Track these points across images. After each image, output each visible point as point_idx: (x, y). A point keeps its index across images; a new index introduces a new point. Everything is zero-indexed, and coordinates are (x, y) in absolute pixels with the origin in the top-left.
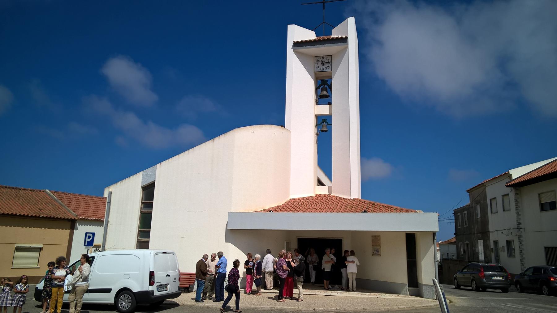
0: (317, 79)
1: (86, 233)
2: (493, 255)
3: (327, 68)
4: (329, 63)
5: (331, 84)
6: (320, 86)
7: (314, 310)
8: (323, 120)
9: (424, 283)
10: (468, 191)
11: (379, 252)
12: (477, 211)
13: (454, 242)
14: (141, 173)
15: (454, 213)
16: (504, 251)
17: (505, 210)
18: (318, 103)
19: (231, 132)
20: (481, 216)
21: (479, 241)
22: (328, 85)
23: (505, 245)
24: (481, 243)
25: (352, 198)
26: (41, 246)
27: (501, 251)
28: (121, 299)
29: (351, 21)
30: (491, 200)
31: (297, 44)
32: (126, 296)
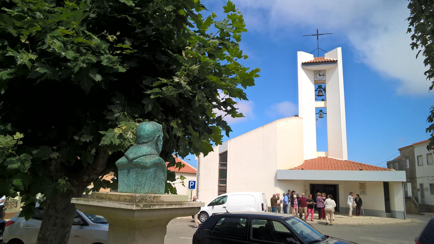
1: (190, 182)
2: (419, 194)
4: (324, 75)
7: (346, 224)
9: (396, 210)
10: (399, 150)
11: (365, 192)
12: (406, 163)
15: (387, 164)
16: (428, 191)
17: (429, 163)
18: (316, 100)
19: (274, 122)
20: (409, 167)
21: (407, 183)
22: (322, 88)
23: (429, 187)
25: (344, 160)
27: (425, 190)
28: (201, 217)
29: (339, 49)
30: (418, 157)
31: (304, 64)
32: (205, 216)
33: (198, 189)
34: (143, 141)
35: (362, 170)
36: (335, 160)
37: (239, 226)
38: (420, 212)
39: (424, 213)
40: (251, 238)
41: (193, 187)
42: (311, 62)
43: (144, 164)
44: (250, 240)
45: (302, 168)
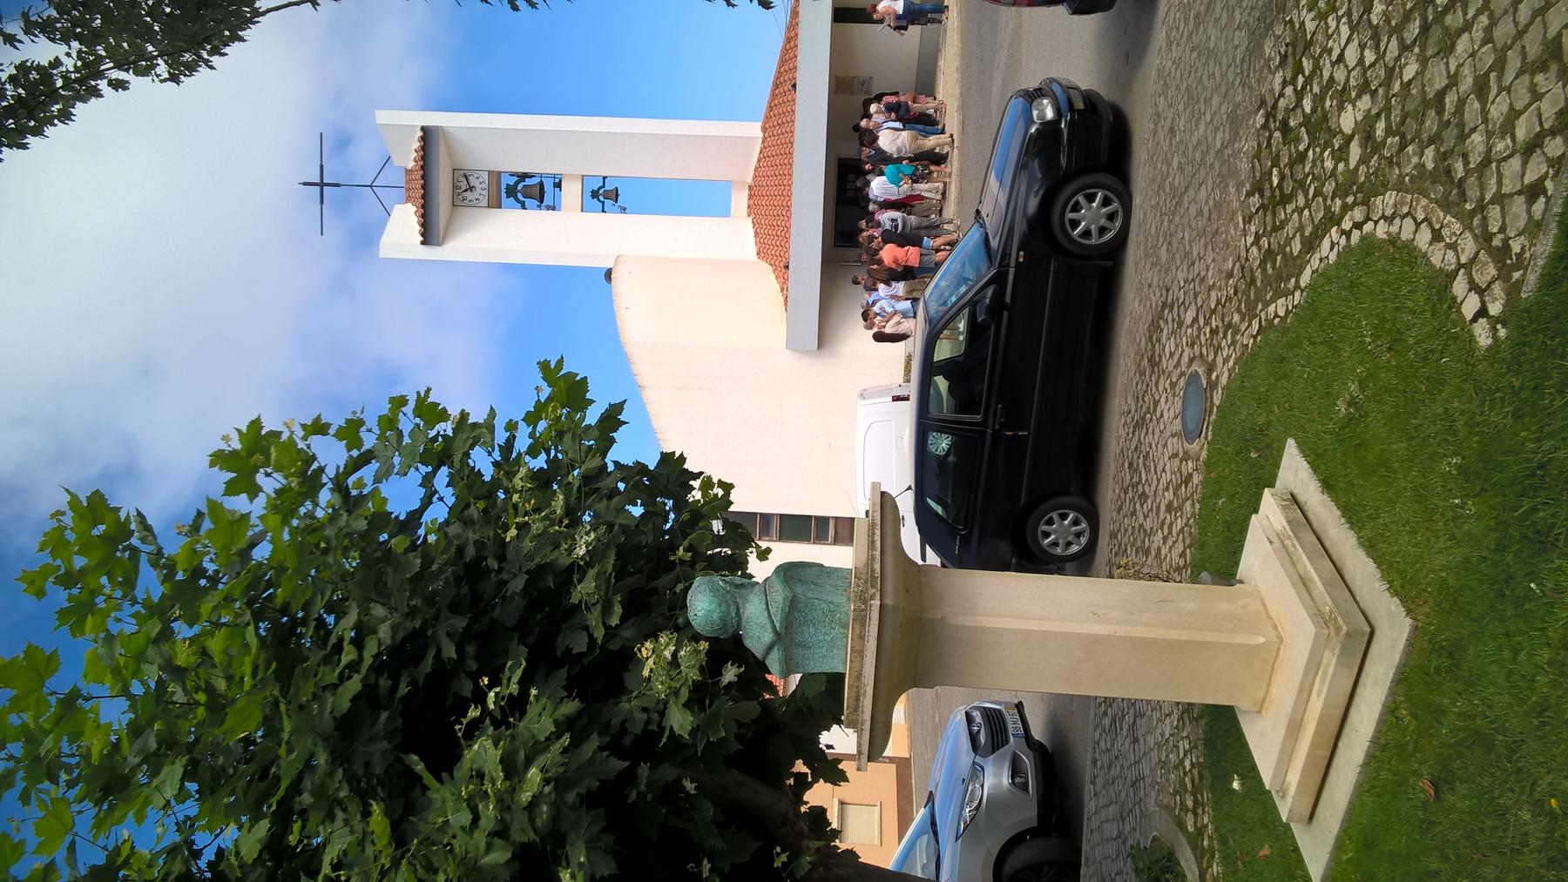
6: (517, 200)
22: (517, 183)
26: (836, 801)
34: (734, 615)
35: (793, 82)
36: (759, 161)
37: (951, 458)
40: (978, 418)
42: (423, 216)
43: (787, 604)
44: (984, 423)
45: (783, 268)
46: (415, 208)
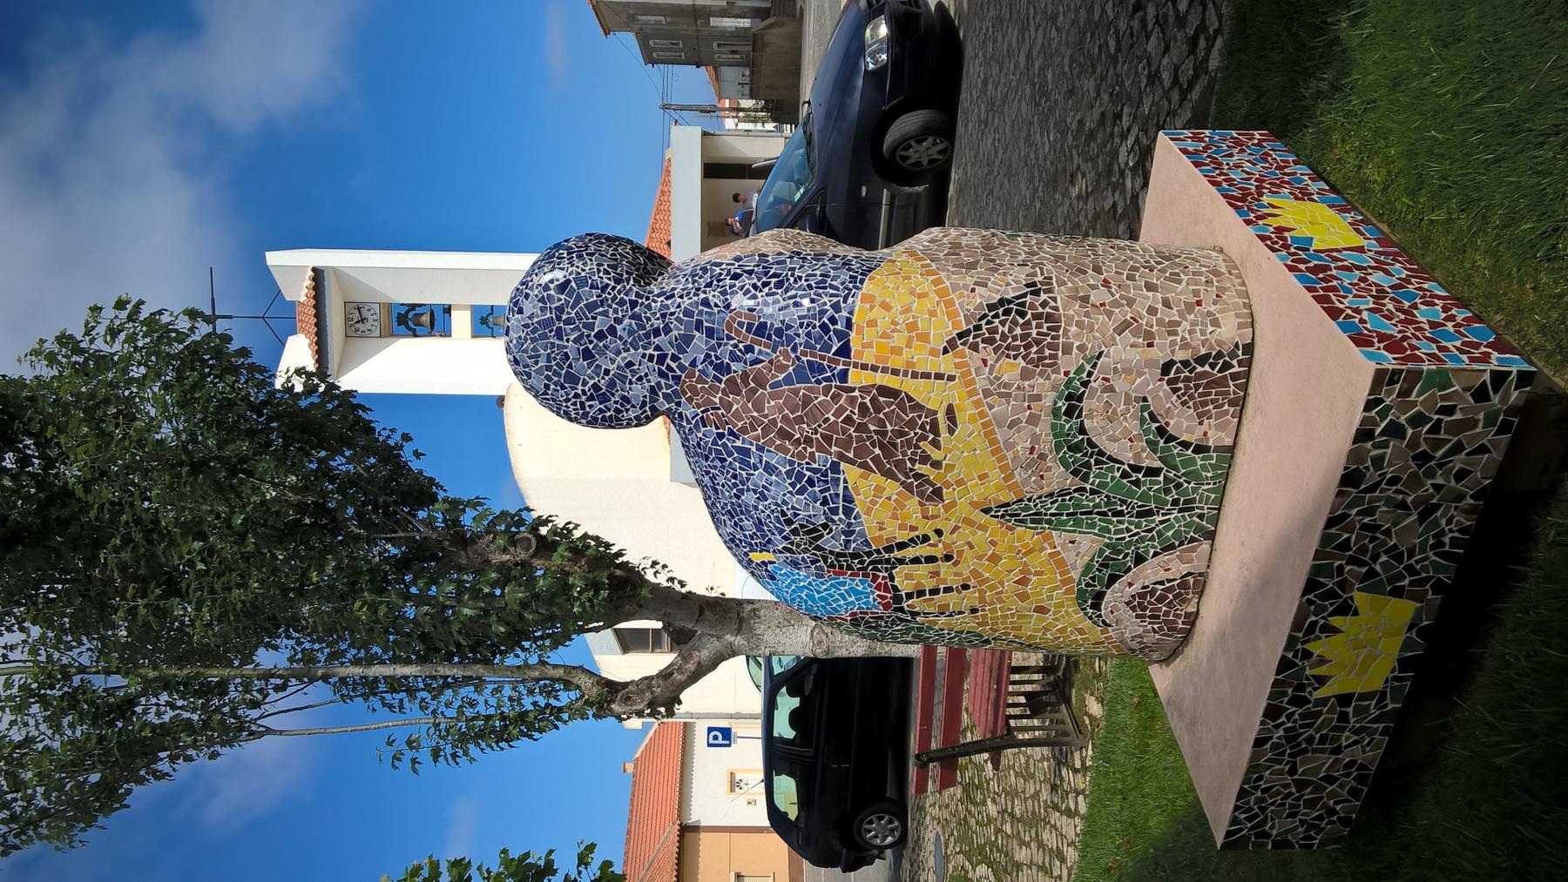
0: (393, 335)
1: (709, 745)
3: (372, 312)
4: (359, 309)
5: (408, 305)
6: (408, 328)
8: (482, 324)
13: (716, 69)
14: (597, 658)
18: (446, 333)
19: (520, 485)
22: (407, 312)
24: (714, 22)
26: (732, 875)
29: (274, 258)
33: (731, 717)
38: (794, 16)
39: (798, 7)
41: (726, 733)
46: (308, 341)
